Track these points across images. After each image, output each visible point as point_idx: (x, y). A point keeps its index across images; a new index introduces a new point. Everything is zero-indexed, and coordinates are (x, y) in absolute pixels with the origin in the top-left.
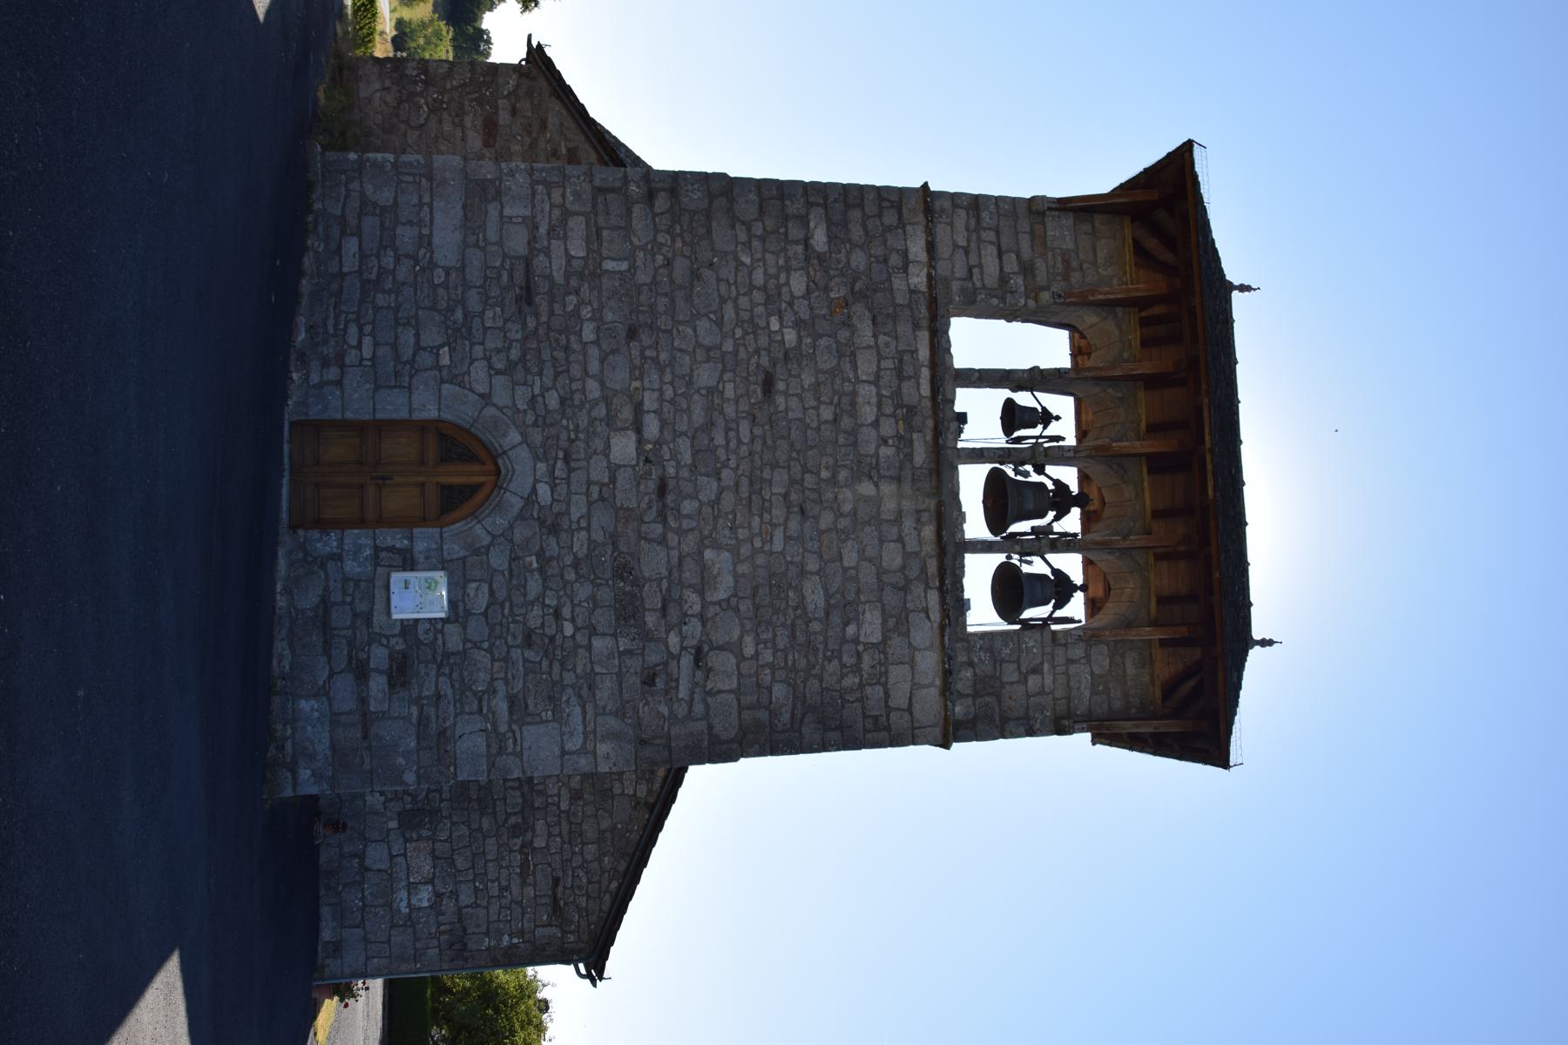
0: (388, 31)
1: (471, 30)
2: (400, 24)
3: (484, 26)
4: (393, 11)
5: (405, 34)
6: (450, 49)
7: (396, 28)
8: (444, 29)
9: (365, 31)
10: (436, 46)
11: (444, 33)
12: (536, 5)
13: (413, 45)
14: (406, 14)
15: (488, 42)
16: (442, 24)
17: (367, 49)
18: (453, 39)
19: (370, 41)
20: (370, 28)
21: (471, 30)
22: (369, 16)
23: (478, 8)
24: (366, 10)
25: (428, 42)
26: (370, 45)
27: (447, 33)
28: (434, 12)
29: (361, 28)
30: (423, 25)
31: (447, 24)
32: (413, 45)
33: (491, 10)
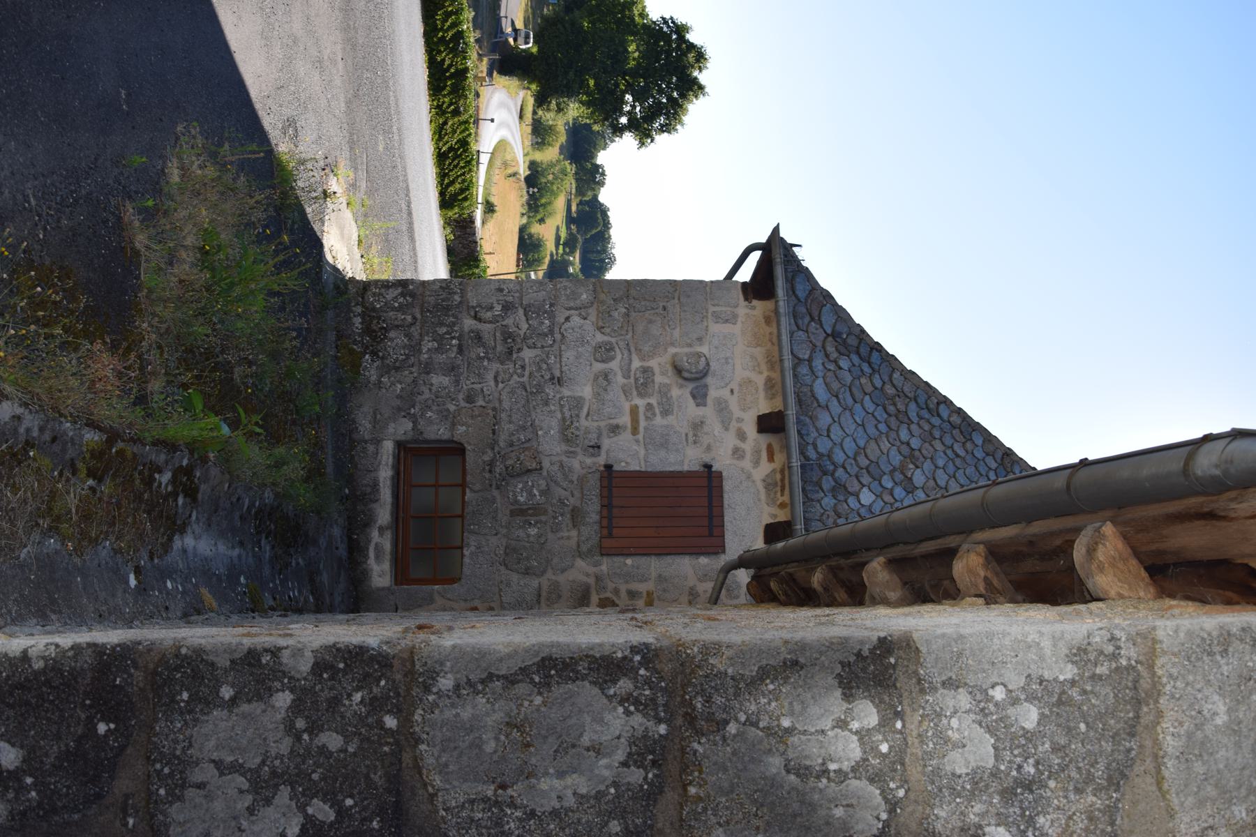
0: (521, 172)
1: (589, 166)
2: (533, 165)
3: (600, 160)
4: (525, 155)
5: (537, 172)
6: (573, 182)
7: (529, 168)
8: (569, 167)
9: (458, 186)
10: (562, 180)
11: (569, 170)
12: (652, 141)
13: (543, 180)
14: (538, 156)
15: (603, 174)
16: (567, 163)
17: (463, 209)
18: (576, 173)
19: (466, 199)
20: (464, 181)
21: (589, 166)
22: (462, 164)
23: (595, 148)
24: (456, 157)
25: (556, 178)
26: (466, 204)
27: (570, 168)
28: (560, 154)
29: (452, 183)
30: (551, 165)
31: (571, 164)
32: (543, 180)
33: (604, 149)
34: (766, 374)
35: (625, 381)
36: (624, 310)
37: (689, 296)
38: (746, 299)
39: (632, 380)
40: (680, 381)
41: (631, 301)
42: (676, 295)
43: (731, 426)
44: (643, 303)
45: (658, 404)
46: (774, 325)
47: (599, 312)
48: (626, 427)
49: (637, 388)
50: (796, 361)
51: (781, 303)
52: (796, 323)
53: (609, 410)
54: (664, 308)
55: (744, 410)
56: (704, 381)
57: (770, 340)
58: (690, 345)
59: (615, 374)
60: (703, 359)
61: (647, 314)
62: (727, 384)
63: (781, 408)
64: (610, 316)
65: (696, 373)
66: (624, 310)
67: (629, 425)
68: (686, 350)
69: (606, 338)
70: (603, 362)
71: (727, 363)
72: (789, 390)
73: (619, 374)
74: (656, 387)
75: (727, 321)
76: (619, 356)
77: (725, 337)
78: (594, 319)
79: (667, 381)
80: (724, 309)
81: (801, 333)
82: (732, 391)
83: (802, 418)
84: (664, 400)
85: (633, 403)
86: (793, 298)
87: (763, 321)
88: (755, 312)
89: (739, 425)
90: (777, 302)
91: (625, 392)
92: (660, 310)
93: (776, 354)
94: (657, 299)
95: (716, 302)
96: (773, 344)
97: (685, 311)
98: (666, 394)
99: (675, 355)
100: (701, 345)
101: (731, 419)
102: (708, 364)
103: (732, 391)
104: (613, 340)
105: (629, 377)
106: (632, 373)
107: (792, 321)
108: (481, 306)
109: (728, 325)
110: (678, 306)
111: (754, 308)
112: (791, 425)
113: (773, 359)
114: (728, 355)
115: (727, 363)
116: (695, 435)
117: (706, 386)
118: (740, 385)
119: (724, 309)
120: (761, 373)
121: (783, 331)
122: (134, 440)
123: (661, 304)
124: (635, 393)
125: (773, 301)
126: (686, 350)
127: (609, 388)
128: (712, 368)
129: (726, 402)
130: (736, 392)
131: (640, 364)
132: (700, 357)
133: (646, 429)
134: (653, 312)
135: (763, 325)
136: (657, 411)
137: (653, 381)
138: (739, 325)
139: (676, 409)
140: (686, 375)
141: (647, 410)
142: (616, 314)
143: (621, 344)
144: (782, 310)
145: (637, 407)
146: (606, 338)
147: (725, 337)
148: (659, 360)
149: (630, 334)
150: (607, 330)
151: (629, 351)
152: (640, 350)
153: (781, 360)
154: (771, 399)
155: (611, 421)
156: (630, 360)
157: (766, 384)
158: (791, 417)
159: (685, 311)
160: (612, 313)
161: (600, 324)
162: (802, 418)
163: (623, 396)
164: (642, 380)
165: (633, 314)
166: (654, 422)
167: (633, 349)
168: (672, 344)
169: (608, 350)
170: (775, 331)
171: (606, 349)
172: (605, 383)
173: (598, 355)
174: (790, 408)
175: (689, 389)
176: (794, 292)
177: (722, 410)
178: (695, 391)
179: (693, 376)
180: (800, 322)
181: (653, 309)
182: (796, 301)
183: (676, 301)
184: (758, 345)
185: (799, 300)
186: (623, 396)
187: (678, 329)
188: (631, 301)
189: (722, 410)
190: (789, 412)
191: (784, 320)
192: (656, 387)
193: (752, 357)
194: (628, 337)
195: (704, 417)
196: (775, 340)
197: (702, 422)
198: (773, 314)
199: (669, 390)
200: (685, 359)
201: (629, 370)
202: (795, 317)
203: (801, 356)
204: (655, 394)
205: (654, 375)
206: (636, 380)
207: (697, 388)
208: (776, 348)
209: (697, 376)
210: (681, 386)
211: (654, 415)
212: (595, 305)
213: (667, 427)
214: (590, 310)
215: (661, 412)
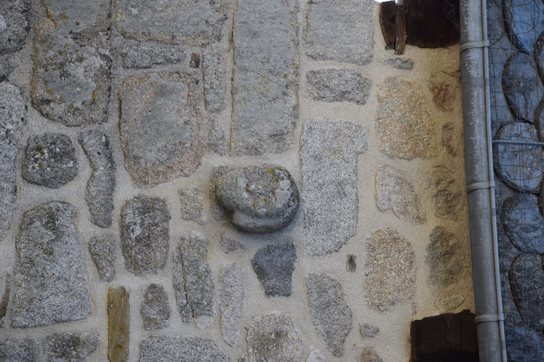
34: (433, 222)
35: (98, 231)
36: (98, 62)
37: (255, 34)
38: (391, 44)
39: (115, 230)
40: (230, 235)
41: (117, 41)
42: (226, 30)
43: (347, 346)
44: (145, 47)
45: (176, 287)
46: (457, 105)
47: (36, 63)
48: (96, 344)
49: (125, 248)
50: (508, 194)
51: (475, 56)
52: (509, 103)
53: (57, 300)
54: (197, 61)
55: (378, 307)
56: (285, 235)
57: (447, 144)
58: (254, 151)
59: (75, 215)
60: (285, 184)
61: (155, 73)
62: (339, 246)
63: (469, 305)
64: (65, 74)
65: (268, 216)
66: (98, 62)
67: (104, 338)
68: (247, 161)
69: (55, 128)
70: (45, 183)
71: (342, 194)
72: (488, 262)
73: (84, 214)
74: (173, 248)
75: (342, 96)
76: (85, 172)
77: (338, 133)
78: (25, 81)
79: (198, 234)
80: (337, 66)
81: (521, 127)
82: (351, 261)
83: (522, 331)
84: (190, 278)
85: (115, 284)
86: (505, 42)
87: (430, 96)
88: (411, 76)
89: (368, 342)
90: (464, 51)
91: (95, 258)
92: (186, 66)
93: (459, 175)
94: (180, 38)
95: (319, 49)
96: (451, 151)
97: (245, 70)
98: (194, 264)
99: (219, 172)
100: (279, 150)
101: (347, 330)
102: (296, 197)
103: (351, 261)
104: (72, 133)
105: (109, 223)
106: (116, 213)
107: (501, 97)
108: (336, 251)
109: (345, 104)
110: (228, 57)
111: (408, 65)
112: (494, 347)
113: (453, 189)
114: (343, 175)
115: (342, 194)
116: (376, 191)
117: (290, 248)
118: (371, 248)
119: (337, 66)
120: (420, 220)
121: (478, 121)
122: (47, 273)
123: (189, 52)
124: (120, 260)
125: (455, 49)
126: (247, 161)
127: (57, 248)
128: (306, 206)
129: (337, 286)
130: (360, 264)
131: (137, 192)
132: (278, 179)
133: (144, 347)
134: (167, 68)
135: (430, 105)
136: (173, 305)
137: (165, 233)
138: (372, 104)
139: (217, 301)
140: (243, 220)
141: (148, 302)
142: (78, 71)
143: (92, 142)
144: (475, 72)
145: (124, 293)
146: (55, 128)
147: (338, 133)
148: (181, 182)
149: (114, 119)
150: (58, 109)
151: (110, 159)
152: (136, 158)
153: (471, 192)
154: (446, 282)
155: (61, 329)
156: (113, 182)
157: (432, 247)
158: (493, 328)
159: (245, 70)
160: (70, 68)
161: (41, 92)
162: (522, 331)
163: (91, 269)
164: (138, 231)
165: (121, 73)
166: (163, 332)
167: (118, 156)
168: (213, 147)
169: (59, 157)
170: (458, 122)
171: (54, 155)
172: (49, 235)
173: (33, 168)
174: (491, 307)
175: (250, 255)
176: (507, 29)
177: (328, 305)
178: (263, 261)
179: (260, 223)
180: (520, 101)
181: (169, 61)
182: (511, 50)
183: (225, 44)
184: (416, 155)
185: (520, 48)
186: (91, 268)
187: (227, 112)
188: (117, 41)
189: (328, 305)
190: (490, 317)
191: (477, 94)
192: (173, 248)
193: (401, 181)
194: (107, 126)
195: (283, 321)
196: (456, 142)
197: (278, 334)
198: (453, 82)
199: (204, 256)
200: (242, 182)
201: (109, 207)
202: (507, 88)
203: (520, 183)
204: (170, 265)
205: (167, 218)
206: (125, 228)
207: (268, 250)
208: (459, 161)
209: (270, 222)
210: (231, 248)
211: (166, 313)
212: (28, 48)
213: (195, 343)
214: (15, 59)
215: (182, 308)
